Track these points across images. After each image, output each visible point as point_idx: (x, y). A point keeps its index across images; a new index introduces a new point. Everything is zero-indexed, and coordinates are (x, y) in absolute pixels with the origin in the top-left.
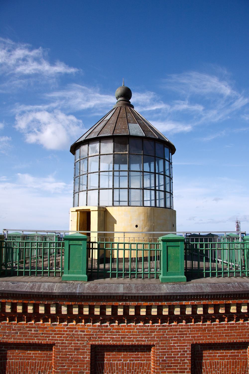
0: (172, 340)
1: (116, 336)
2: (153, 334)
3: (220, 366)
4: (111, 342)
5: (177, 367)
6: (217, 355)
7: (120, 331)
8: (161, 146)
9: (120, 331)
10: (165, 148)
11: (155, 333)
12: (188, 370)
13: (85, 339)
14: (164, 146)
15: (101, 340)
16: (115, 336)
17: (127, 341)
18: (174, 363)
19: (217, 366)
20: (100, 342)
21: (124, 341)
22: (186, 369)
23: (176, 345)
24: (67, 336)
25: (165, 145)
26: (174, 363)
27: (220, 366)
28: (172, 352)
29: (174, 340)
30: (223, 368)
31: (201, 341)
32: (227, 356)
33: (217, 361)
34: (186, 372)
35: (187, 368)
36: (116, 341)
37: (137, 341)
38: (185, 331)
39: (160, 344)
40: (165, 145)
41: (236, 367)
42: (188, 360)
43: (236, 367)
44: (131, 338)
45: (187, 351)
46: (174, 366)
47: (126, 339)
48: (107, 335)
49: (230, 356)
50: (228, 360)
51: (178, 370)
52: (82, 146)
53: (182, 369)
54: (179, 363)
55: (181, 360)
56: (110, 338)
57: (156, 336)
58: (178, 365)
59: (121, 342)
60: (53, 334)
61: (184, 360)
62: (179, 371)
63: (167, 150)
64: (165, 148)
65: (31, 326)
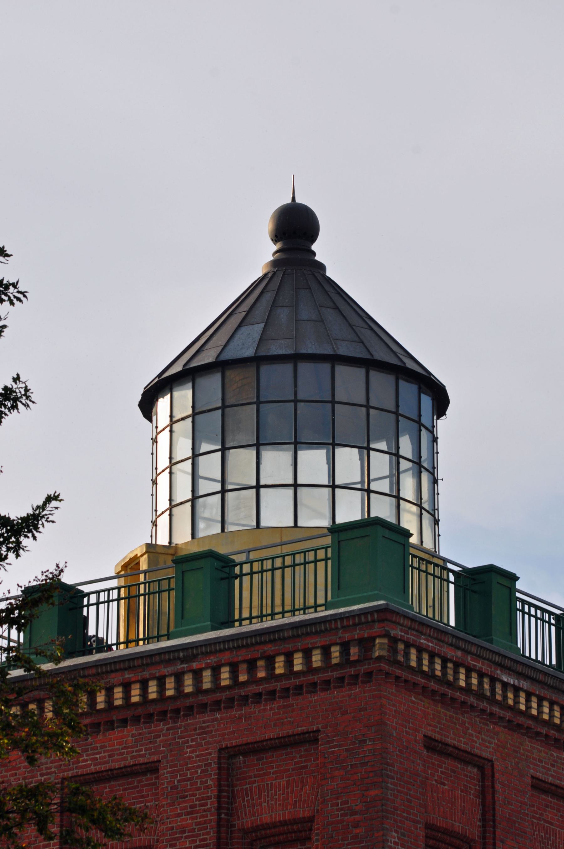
0: (188, 747)
1: (101, 755)
2: (158, 740)
3: (276, 792)
4: (92, 767)
5: (194, 798)
6: (272, 771)
7: (107, 744)
8: (414, 388)
9: (107, 744)
10: (423, 396)
11: (161, 738)
12: (213, 800)
13: (53, 770)
14: (420, 388)
15: (76, 768)
16: (98, 756)
17: (118, 761)
18: (190, 790)
19: (270, 792)
20: (75, 771)
21: (112, 762)
22: (209, 798)
23: (193, 755)
24: (24, 770)
25: (422, 386)
26: (190, 790)
27: (276, 792)
28: (188, 769)
29: (191, 746)
30: (279, 795)
31: (234, 741)
32: (288, 770)
33: (252, 774)
34: (209, 803)
35: (211, 796)
36: (100, 764)
37: (133, 757)
38: (208, 726)
39: (169, 758)
40: (422, 386)
41: (301, 789)
42: (212, 780)
43: (301, 789)
44: (123, 753)
45: (211, 764)
46: (190, 795)
47: (116, 757)
48: (87, 755)
49: (293, 769)
50: (290, 777)
51: (197, 803)
52: (415, 481)
53: (203, 799)
54: (199, 789)
55: (202, 783)
56: (92, 759)
57: (162, 744)
58: (198, 792)
59: (107, 765)
60: (3, 772)
61: (206, 782)
62: (199, 804)
63: (427, 402)
64: (423, 396)
65: (174, 842)
